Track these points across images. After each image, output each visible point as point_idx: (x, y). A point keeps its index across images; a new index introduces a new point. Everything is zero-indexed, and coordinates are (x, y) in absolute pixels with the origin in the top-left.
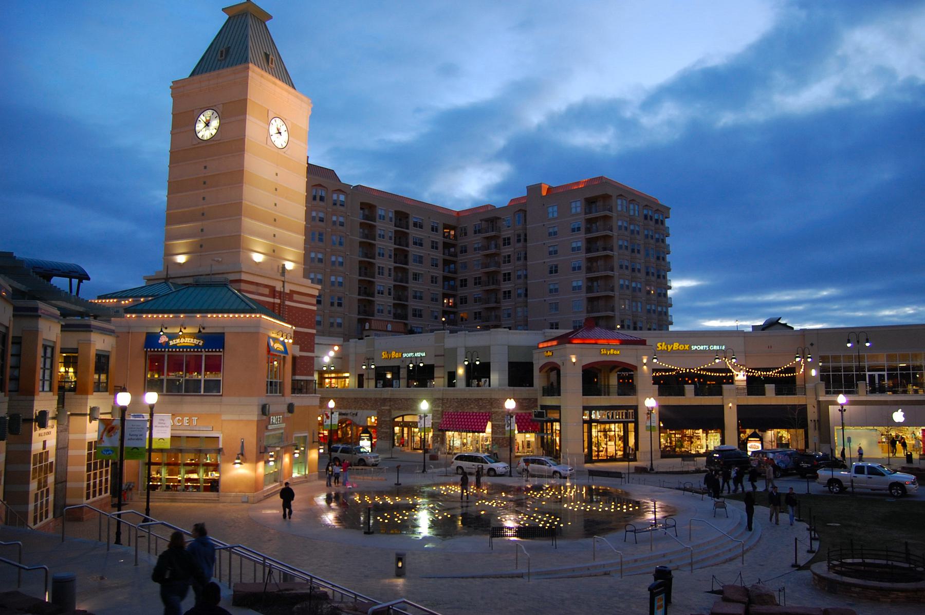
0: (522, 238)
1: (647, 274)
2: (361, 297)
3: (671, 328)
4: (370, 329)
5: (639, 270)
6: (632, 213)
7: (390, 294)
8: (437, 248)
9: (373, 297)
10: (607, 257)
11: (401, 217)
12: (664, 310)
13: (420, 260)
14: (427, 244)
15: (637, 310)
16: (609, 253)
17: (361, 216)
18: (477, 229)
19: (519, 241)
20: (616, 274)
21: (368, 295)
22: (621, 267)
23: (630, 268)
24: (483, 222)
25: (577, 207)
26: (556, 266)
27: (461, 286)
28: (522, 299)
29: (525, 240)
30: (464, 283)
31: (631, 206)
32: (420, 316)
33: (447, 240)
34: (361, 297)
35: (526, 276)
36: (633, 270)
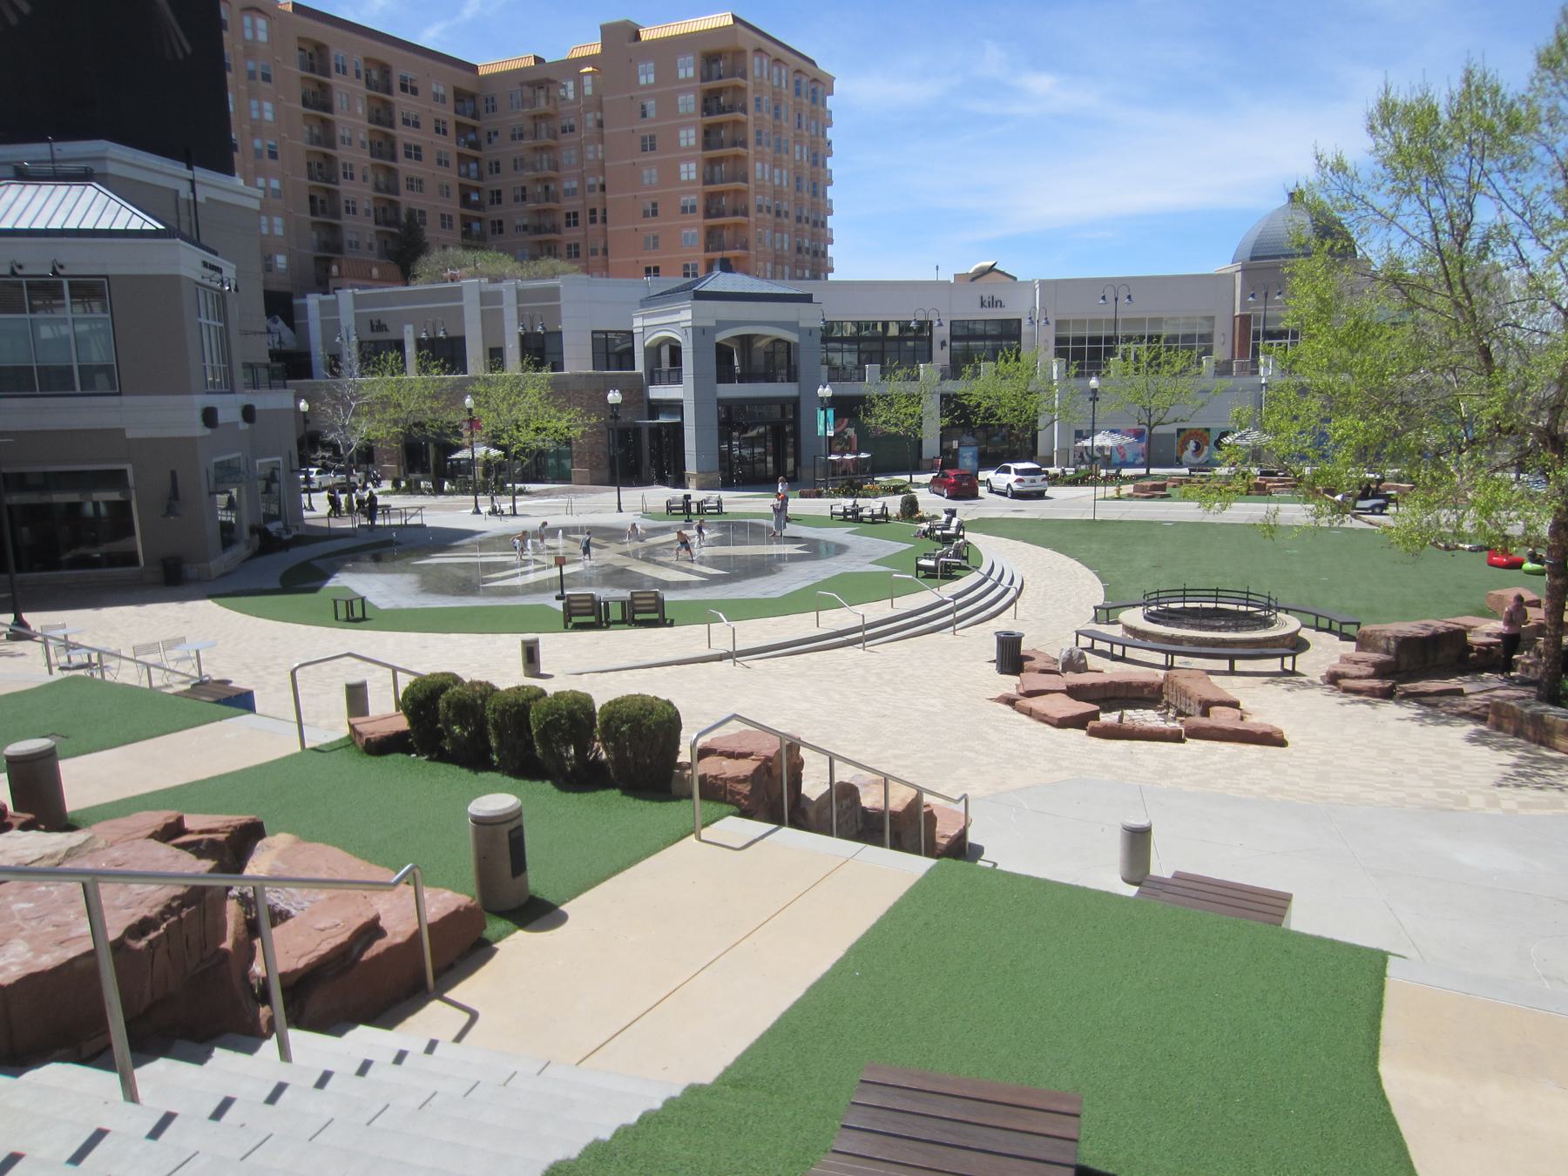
0: (599, 216)
1: (799, 219)
2: (316, 219)
3: (831, 277)
4: (340, 276)
5: (787, 214)
6: (777, 181)
7: (365, 179)
8: (445, 132)
9: (337, 183)
10: (737, 157)
11: (380, 78)
12: (822, 219)
13: (415, 153)
14: (428, 125)
15: (783, 247)
16: (739, 81)
17: (307, 136)
18: (517, 132)
19: (593, 221)
20: (751, 152)
21: (328, 181)
22: (760, 209)
23: (773, 211)
24: (525, 87)
25: (687, 70)
26: (652, 138)
27: (492, 202)
28: (599, 257)
29: (604, 220)
30: (497, 197)
31: (775, 70)
32: (418, 158)
33: (465, 181)
34: (316, 219)
35: (603, 188)
36: (778, 214)
